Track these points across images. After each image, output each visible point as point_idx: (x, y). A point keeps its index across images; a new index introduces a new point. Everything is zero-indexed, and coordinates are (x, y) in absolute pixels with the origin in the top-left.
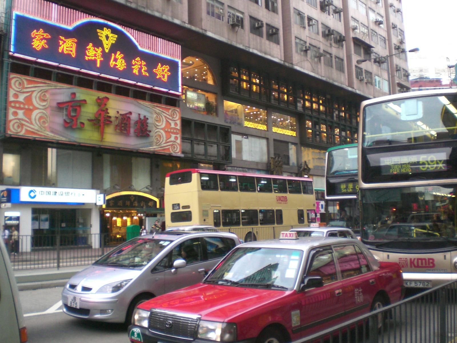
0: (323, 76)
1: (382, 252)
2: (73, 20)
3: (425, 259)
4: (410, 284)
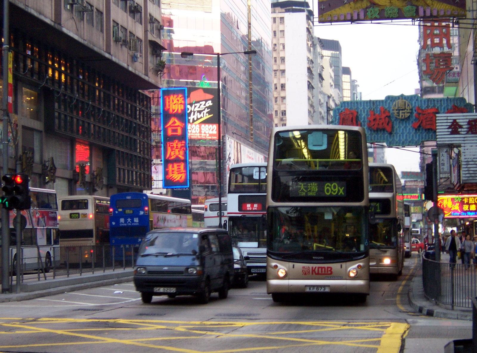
0: (85, 38)
1: (288, 263)
2: (334, 156)
3: (324, 268)
4: (313, 289)
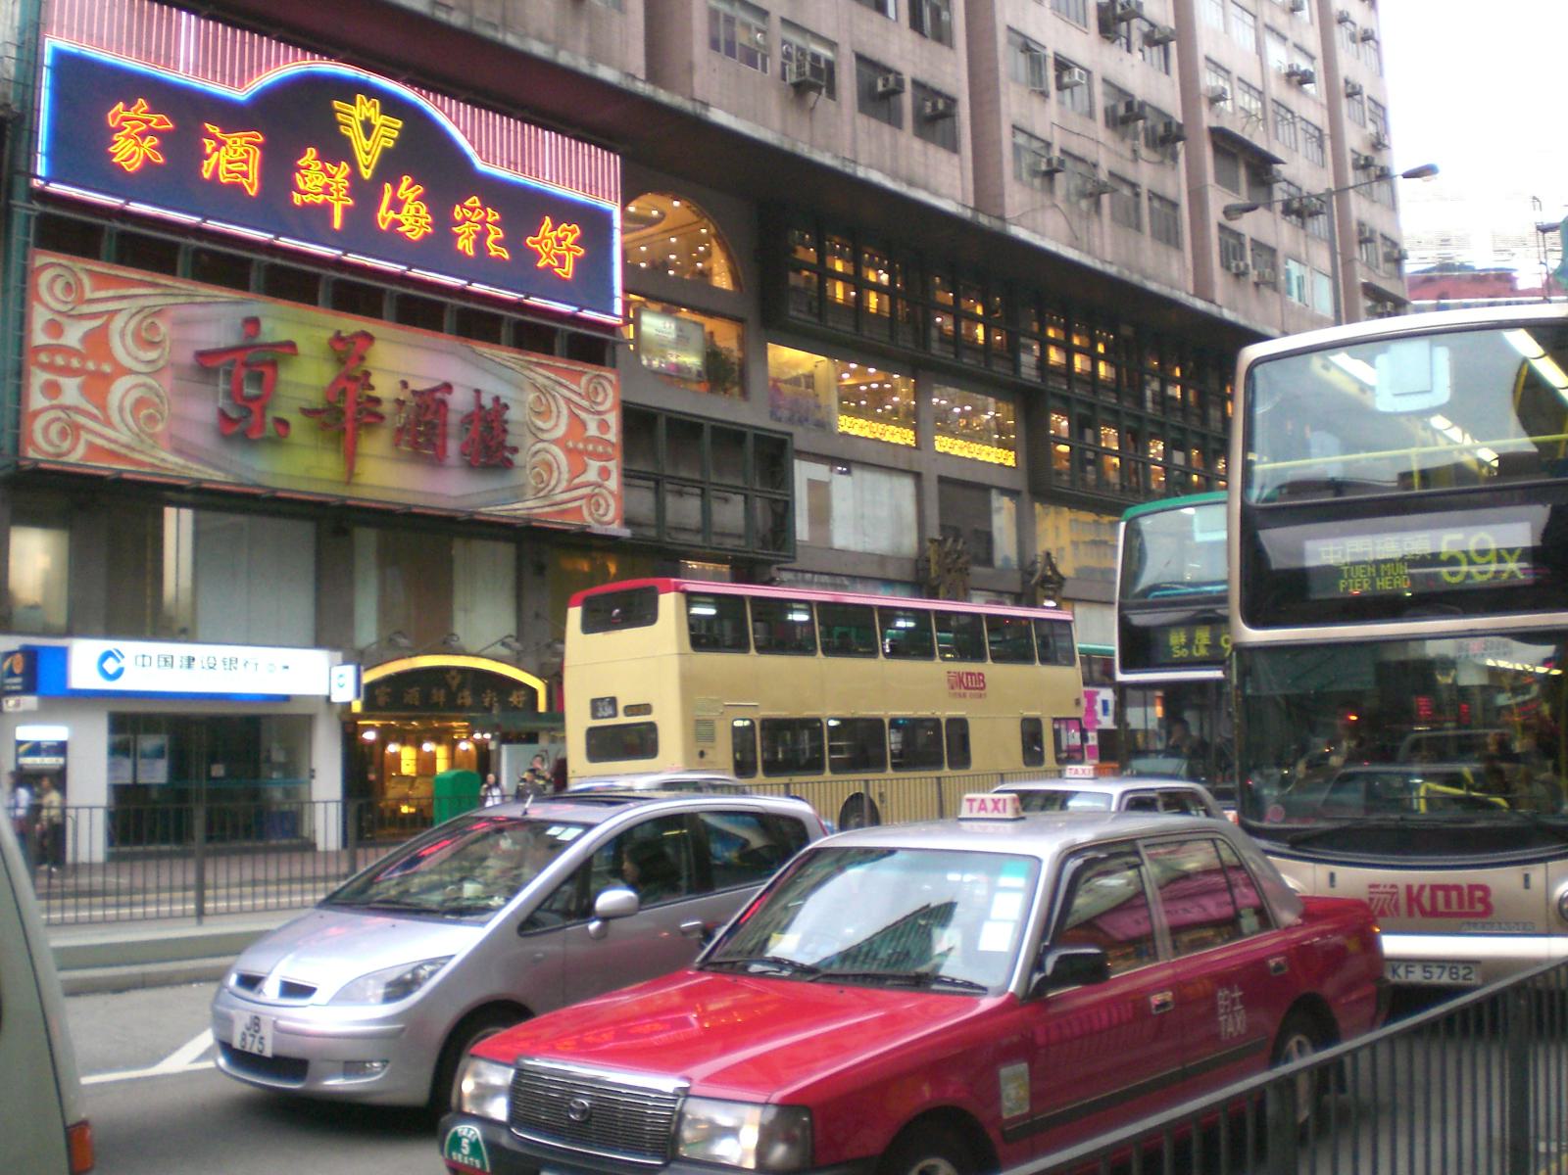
0: (1109, 259)
1: (1311, 864)
2: (251, 67)
3: (1458, 888)
4: (1407, 972)
